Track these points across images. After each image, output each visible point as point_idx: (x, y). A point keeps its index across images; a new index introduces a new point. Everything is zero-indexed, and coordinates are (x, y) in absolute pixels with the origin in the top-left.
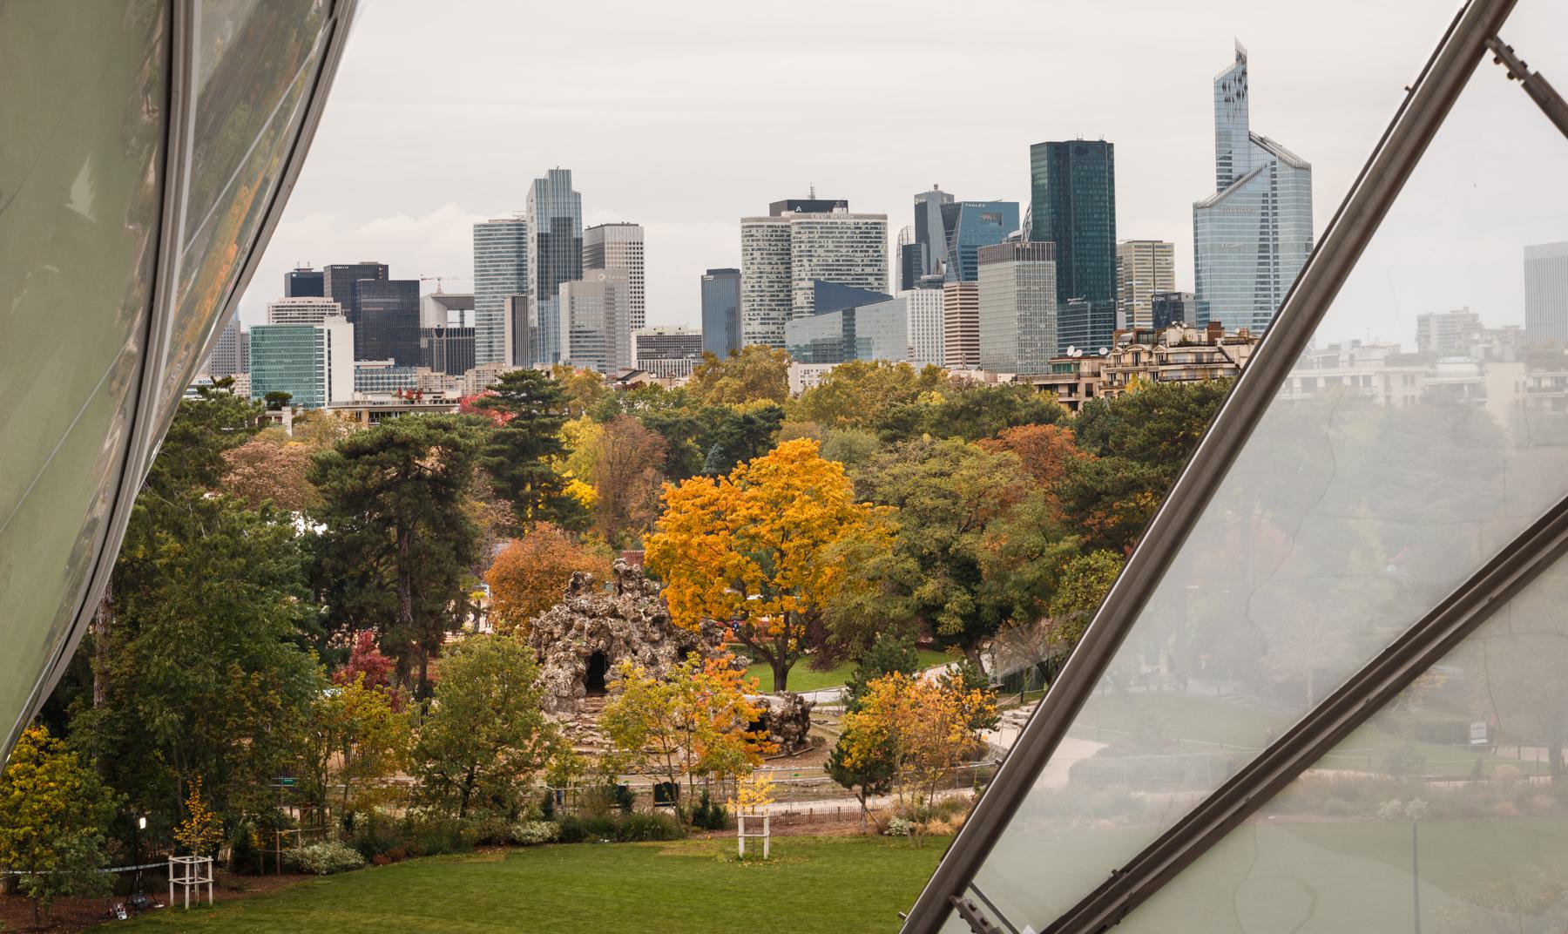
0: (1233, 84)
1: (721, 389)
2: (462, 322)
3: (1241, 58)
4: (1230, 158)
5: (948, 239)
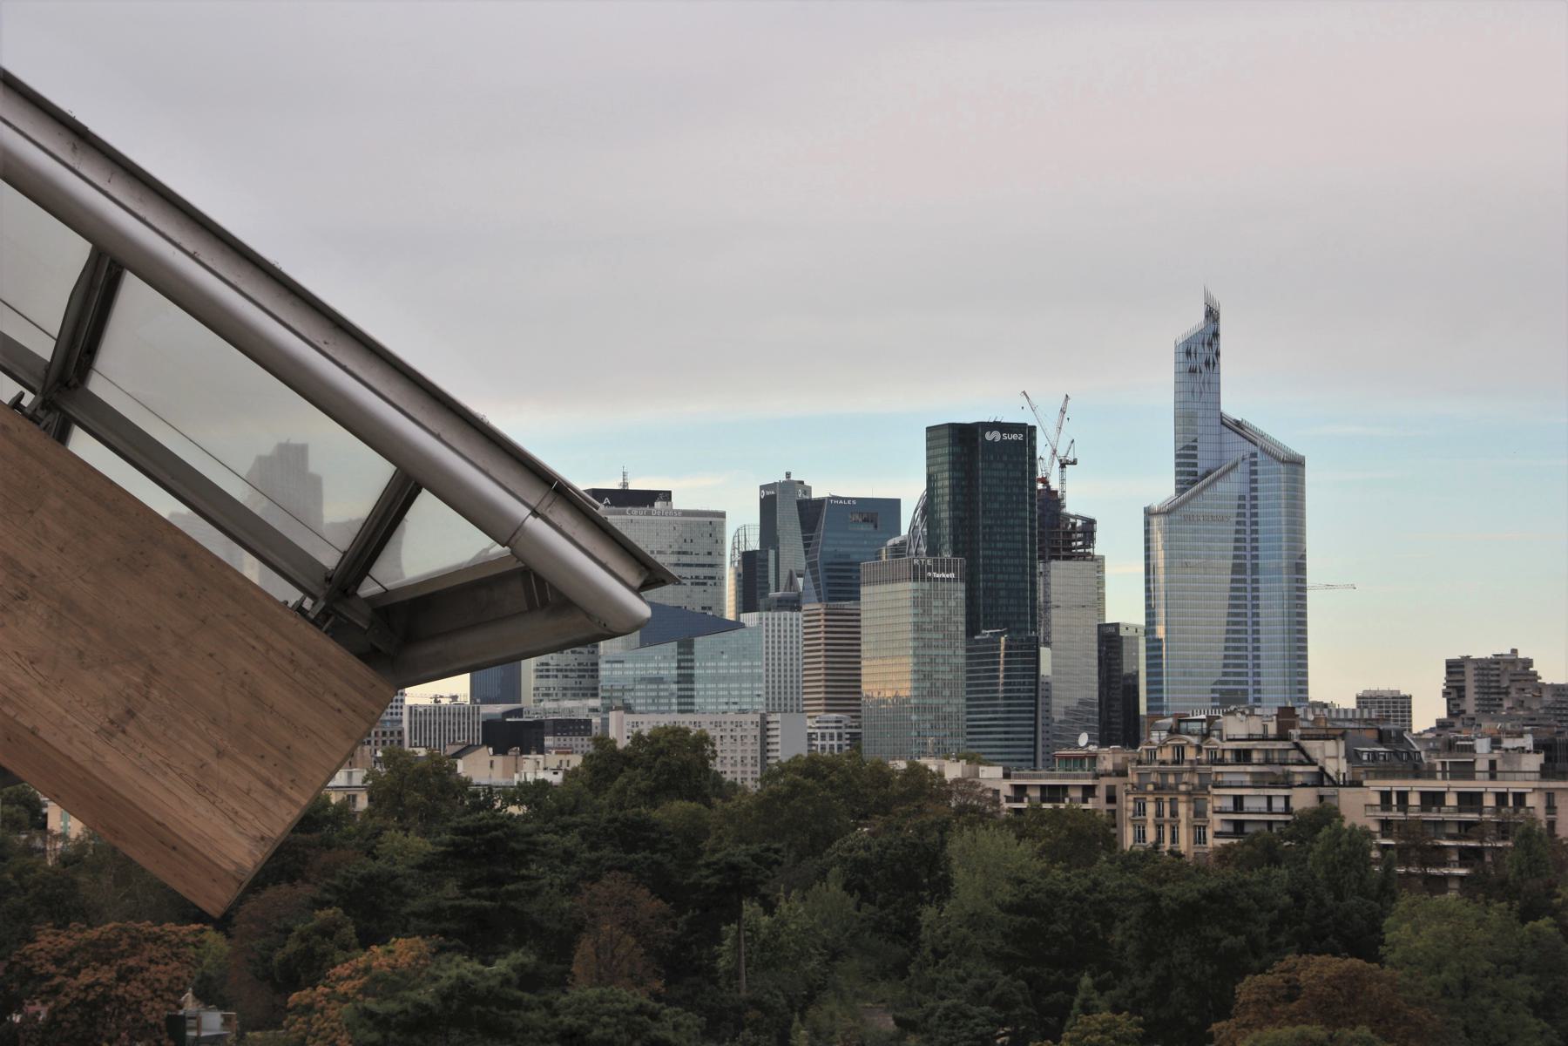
0: (1200, 350)
1: (623, 791)
3: (1212, 315)
4: (1194, 448)
5: (806, 546)
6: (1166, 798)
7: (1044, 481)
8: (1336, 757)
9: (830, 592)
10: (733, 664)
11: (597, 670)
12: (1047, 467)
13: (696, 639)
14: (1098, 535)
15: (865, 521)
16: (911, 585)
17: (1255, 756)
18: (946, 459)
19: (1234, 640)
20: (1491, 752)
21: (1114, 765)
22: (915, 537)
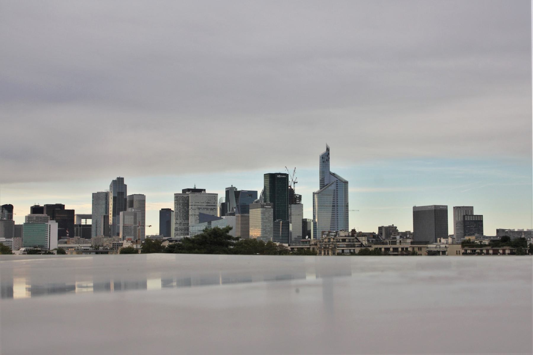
0: (325, 157)
2: (86, 223)
3: (328, 149)
5: (236, 201)
6: (326, 250)
7: (290, 187)
8: (365, 241)
9: (242, 212)
11: (189, 229)
12: (291, 183)
14: (302, 199)
15: (249, 196)
16: (261, 209)
17: (347, 240)
19: (333, 222)
20: (400, 239)
21: (314, 243)
22: (261, 199)
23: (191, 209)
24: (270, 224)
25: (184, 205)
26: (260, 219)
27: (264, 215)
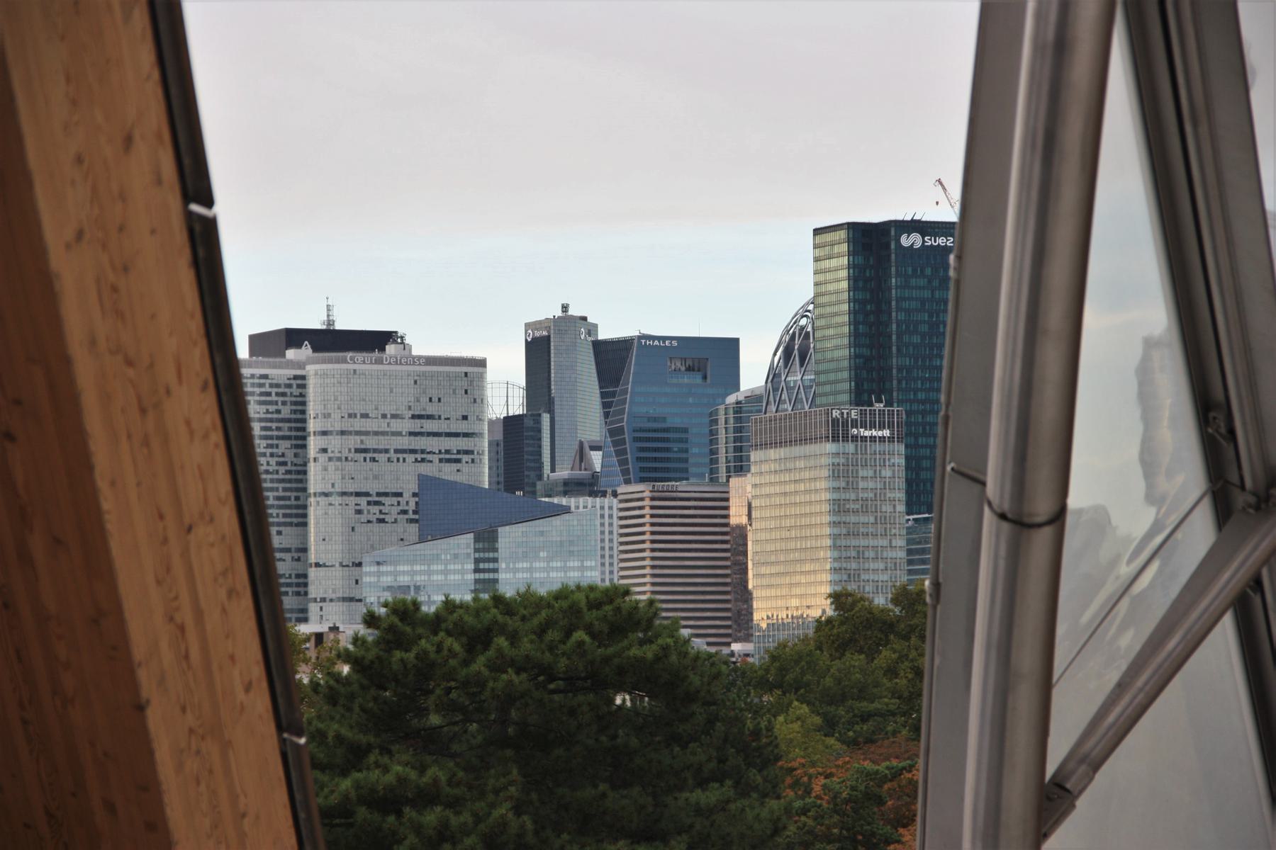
5: (606, 405)
9: (642, 469)
10: (554, 564)
11: (306, 585)
13: (500, 529)
15: (689, 369)
16: (830, 447)
18: (844, 273)
22: (775, 390)
23: (323, 458)
24: (885, 543)
25: (275, 433)
26: (825, 507)
27: (851, 486)
